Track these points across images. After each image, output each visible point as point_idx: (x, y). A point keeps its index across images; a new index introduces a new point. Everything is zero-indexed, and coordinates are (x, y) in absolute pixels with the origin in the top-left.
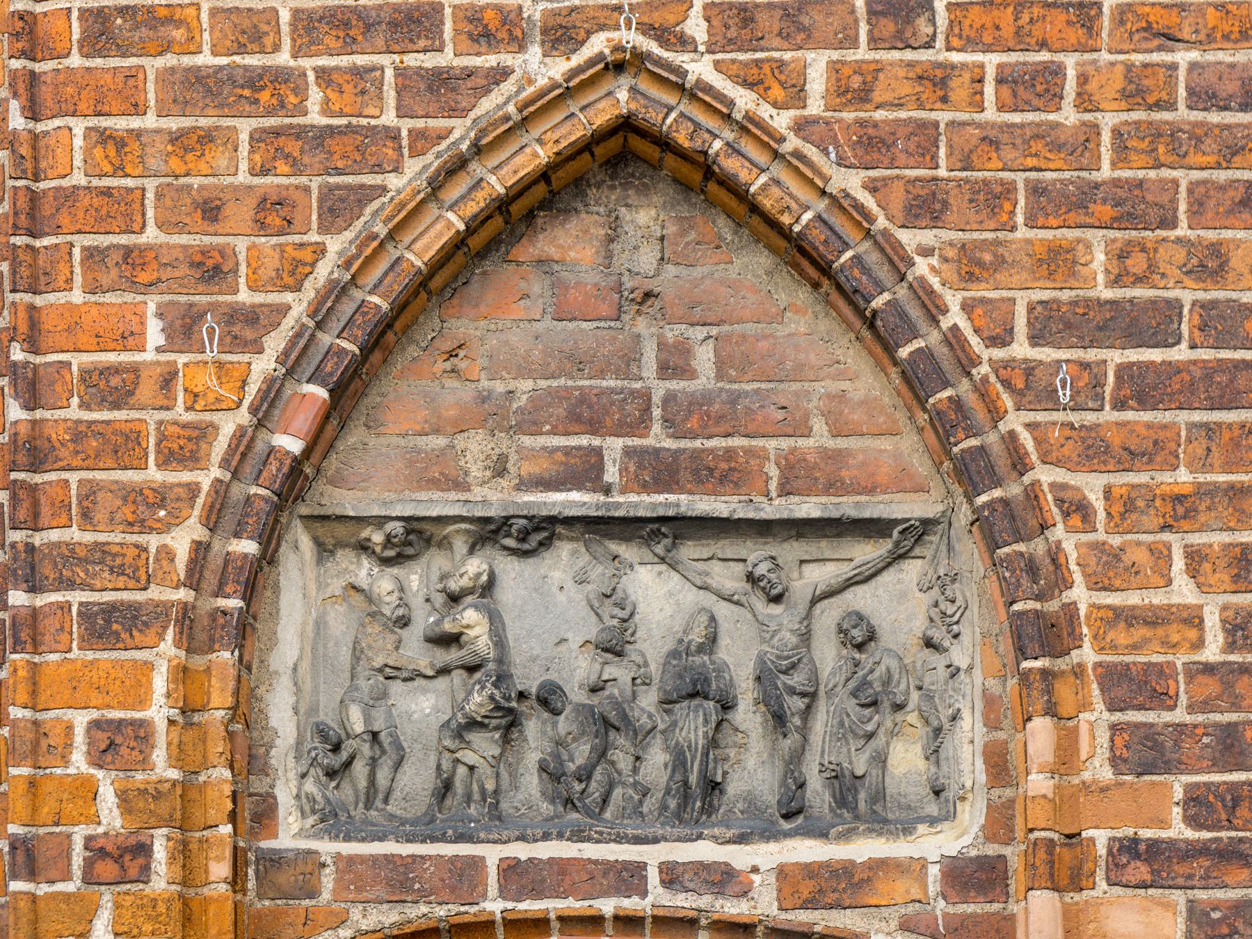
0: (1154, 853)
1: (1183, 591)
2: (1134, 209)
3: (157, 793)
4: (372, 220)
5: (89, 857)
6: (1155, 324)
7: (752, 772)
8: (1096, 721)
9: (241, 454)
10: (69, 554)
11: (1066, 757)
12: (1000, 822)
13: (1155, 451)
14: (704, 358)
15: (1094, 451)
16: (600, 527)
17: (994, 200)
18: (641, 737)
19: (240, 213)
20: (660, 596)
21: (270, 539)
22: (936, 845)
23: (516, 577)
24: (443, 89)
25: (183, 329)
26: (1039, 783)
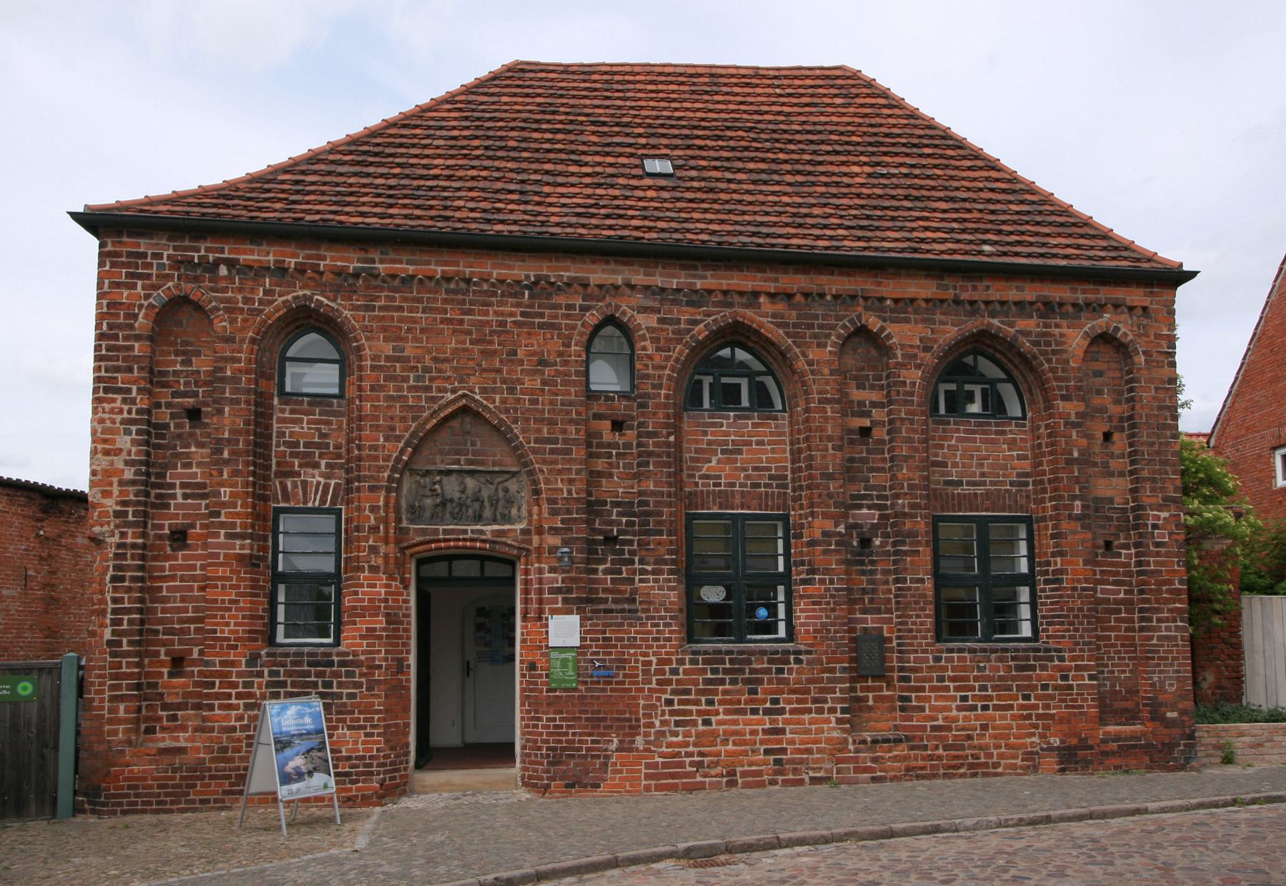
0: (556, 529)
1: (560, 485)
2: (552, 422)
3: (381, 518)
4: (421, 421)
5: (1140, 363)
6: (556, 441)
7: (487, 513)
8: (545, 506)
9: (398, 460)
10: (366, 476)
11: (540, 513)
12: (530, 523)
13: (555, 462)
14: (479, 443)
15: (545, 462)
16: (460, 472)
17: (528, 420)
18: (468, 507)
19: (397, 420)
20: (470, 483)
21: (402, 474)
22: (519, 527)
23: (445, 479)
24: (433, 400)
25: (387, 439)
26: (535, 517)
